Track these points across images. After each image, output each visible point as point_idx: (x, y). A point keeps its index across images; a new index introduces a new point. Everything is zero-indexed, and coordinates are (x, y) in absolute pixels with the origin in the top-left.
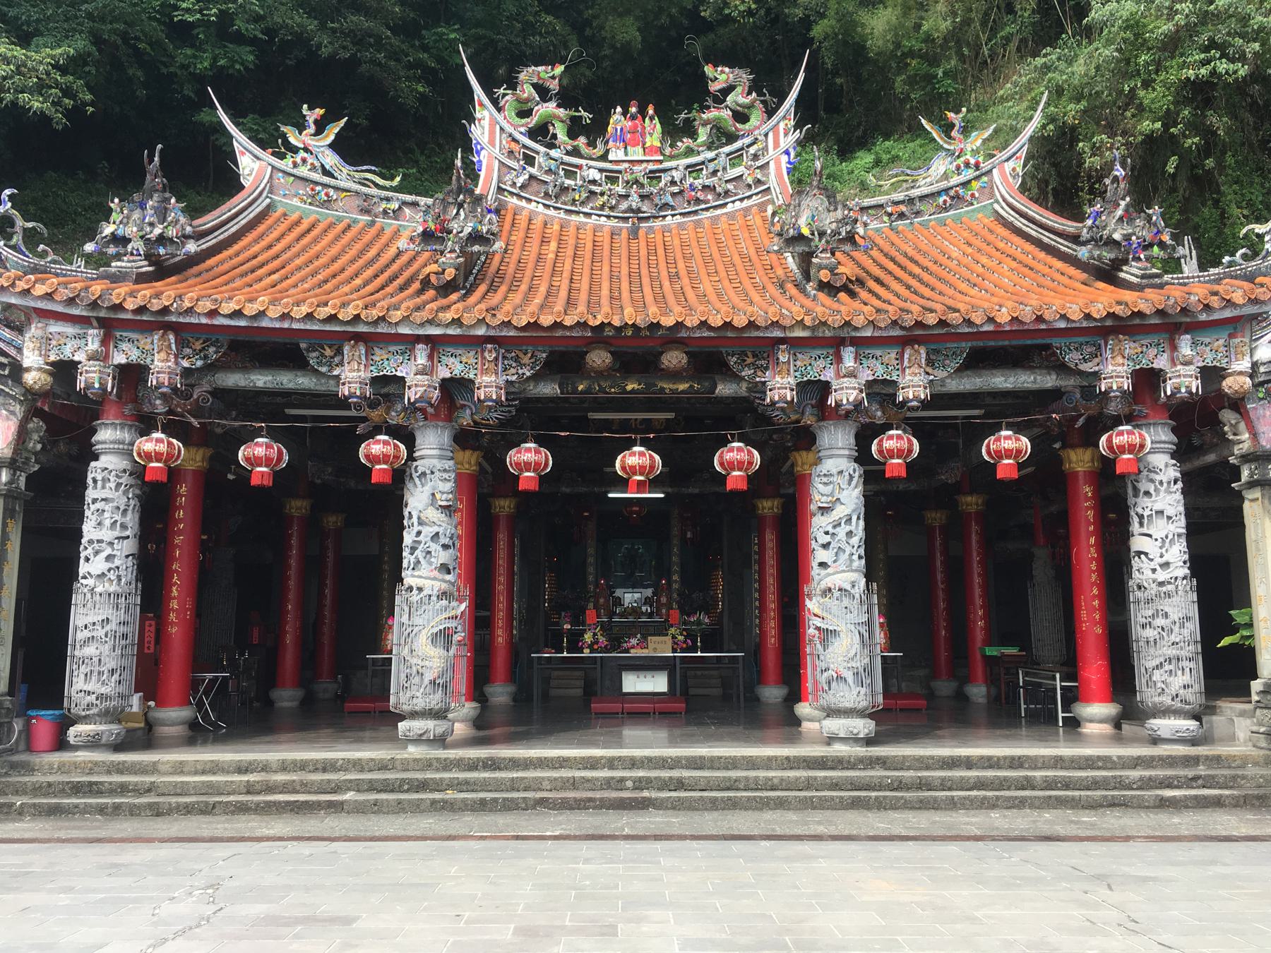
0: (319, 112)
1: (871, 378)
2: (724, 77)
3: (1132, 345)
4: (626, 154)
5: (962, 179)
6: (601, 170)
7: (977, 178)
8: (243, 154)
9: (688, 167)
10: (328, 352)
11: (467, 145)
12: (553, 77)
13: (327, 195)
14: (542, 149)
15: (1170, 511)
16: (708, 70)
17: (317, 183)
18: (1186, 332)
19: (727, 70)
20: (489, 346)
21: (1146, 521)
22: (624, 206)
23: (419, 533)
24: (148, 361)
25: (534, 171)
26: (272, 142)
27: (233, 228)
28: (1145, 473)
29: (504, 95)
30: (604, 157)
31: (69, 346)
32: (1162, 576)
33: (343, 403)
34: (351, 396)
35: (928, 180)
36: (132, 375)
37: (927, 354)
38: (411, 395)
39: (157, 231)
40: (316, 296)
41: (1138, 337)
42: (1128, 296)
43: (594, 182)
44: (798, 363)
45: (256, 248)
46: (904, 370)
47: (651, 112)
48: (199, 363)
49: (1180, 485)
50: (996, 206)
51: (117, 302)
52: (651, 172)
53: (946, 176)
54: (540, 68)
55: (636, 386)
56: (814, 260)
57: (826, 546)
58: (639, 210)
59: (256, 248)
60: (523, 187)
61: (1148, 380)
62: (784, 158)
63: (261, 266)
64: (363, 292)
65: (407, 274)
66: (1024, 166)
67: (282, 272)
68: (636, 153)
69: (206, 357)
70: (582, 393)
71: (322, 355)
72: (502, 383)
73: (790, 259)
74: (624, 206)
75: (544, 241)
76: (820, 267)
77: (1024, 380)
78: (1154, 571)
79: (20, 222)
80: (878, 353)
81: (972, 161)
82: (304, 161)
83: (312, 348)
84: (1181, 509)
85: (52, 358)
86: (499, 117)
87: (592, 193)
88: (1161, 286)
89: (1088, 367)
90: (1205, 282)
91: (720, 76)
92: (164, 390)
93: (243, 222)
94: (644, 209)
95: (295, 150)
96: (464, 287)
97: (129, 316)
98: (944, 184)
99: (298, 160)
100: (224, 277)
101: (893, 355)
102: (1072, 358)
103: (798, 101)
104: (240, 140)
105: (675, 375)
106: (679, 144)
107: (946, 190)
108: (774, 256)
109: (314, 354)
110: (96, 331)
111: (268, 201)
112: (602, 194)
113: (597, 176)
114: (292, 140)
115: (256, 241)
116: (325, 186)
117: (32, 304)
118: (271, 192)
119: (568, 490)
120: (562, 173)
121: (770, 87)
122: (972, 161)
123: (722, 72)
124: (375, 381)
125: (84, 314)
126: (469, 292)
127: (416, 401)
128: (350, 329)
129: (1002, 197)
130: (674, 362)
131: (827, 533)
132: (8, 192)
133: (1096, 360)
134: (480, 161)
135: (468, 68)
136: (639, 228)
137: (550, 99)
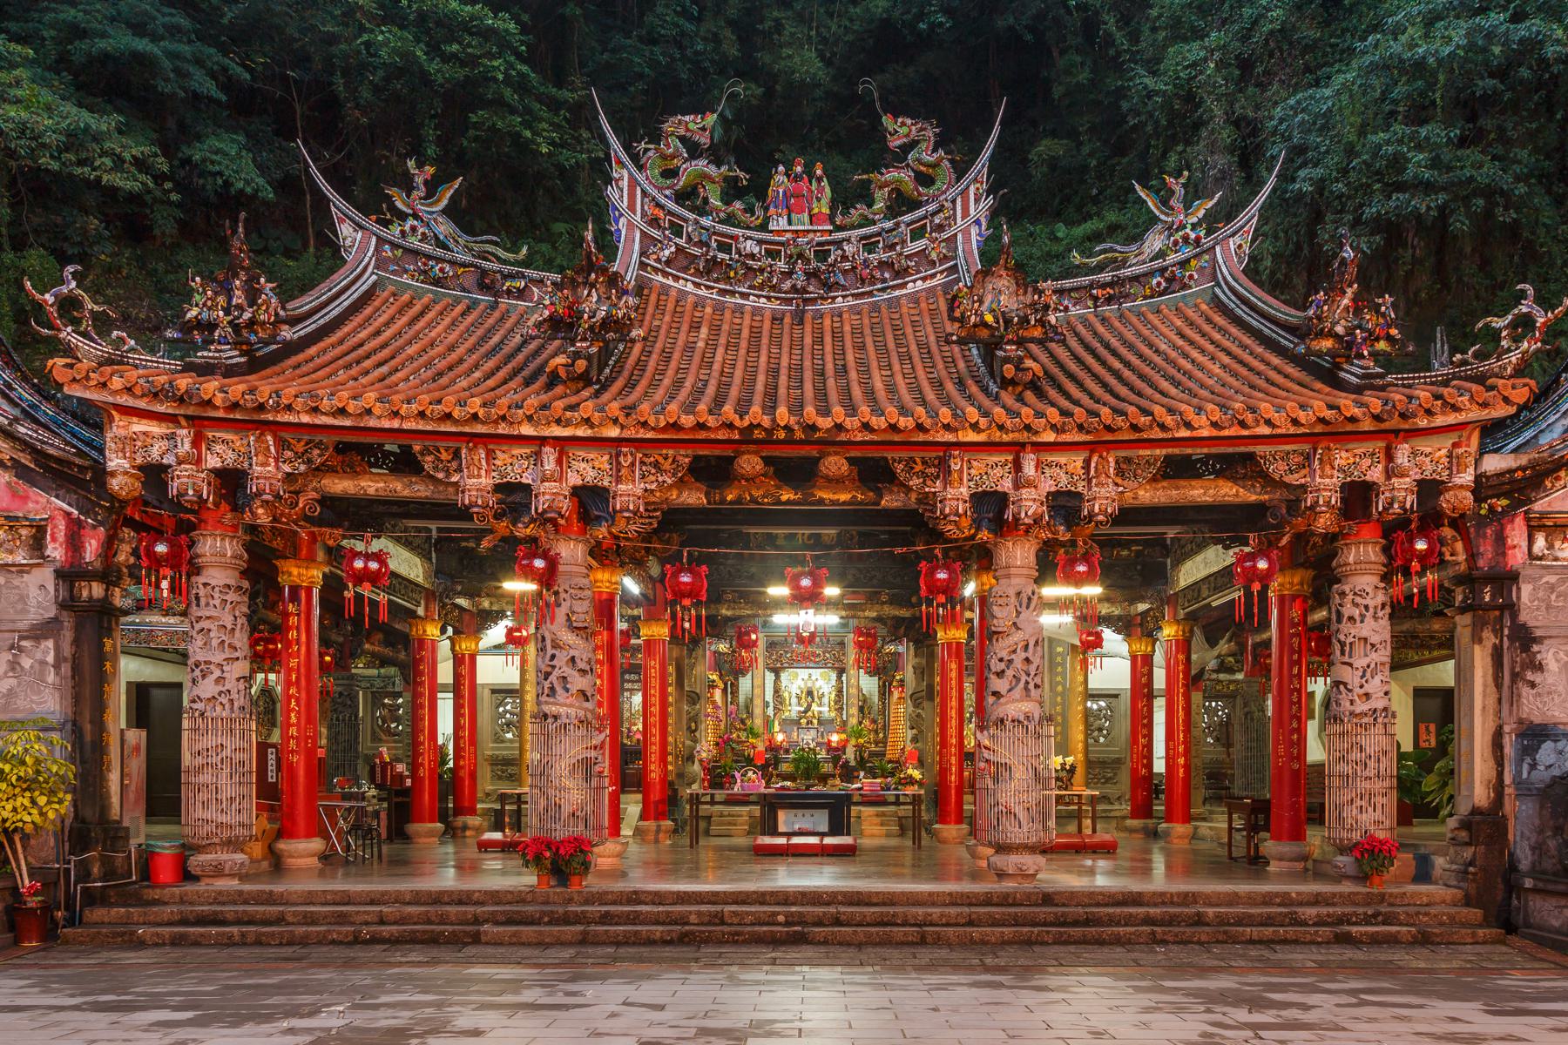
0: (430, 170)
1: (1053, 489)
2: (905, 130)
3: (1344, 454)
4: (790, 223)
5: (1179, 257)
6: (760, 242)
7: (1196, 256)
8: (341, 221)
9: (862, 238)
10: (444, 456)
11: (602, 213)
12: (703, 129)
13: (442, 270)
14: (691, 216)
15: (1375, 639)
16: (887, 121)
17: (429, 257)
18: (1405, 440)
19: (909, 121)
20: (625, 450)
21: (1347, 648)
22: (787, 285)
23: (553, 657)
24: (246, 465)
25: (682, 242)
26: (375, 207)
27: (335, 311)
28: (1351, 597)
29: (646, 150)
30: (763, 227)
31: (156, 447)
32: (1361, 707)
33: (464, 513)
34: (471, 505)
35: (1141, 258)
36: (231, 482)
37: (1117, 462)
38: (542, 503)
39: (247, 315)
40: (429, 391)
41: (1350, 446)
42: (1346, 401)
43: (752, 256)
44: (973, 472)
45: (363, 335)
46: (1090, 481)
47: (819, 172)
48: (303, 468)
49: (1388, 610)
50: (1217, 290)
51: (206, 398)
52: (819, 244)
53: (1161, 254)
54: (687, 118)
55: (792, 497)
56: (1000, 353)
57: (1000, 674)
58: (804, 290)
59: (363, 335)
60: (668, 262)
61: (1357, 496)
62: (974, 231)
63: (368, 356)
64: (483, 387)
65: (533, 366)
66: (1254, 240)
67: (393, 363)
68: (802, 222)
69: (309, 461)
70: (731, 503)
71: (439, 459)
72: (639, 492)
73: (975, 351)
74: (787, 285)
75: (695, 327)
76: (1007, 360)
77: (1227, 492)
78: (1352, 702)
79: (89, 305)
80: (1063, 460)
81: (1193, 236)
82: (414, 229)
83: (426, 451)
84: (1388, 636)
85: (139, 461)
86: (640, 177)
87: (749, 268)
88: (1383, 388)
89: (1295, 479)
90: (1432, 383)
91: (899, 129)
92: (265, 497)
93: (346, 304)
94: (811, 288)
95: (402, 217)
96: (598, 381)
97: (221, 414)
98: (1158, 263)
99: (407, 228)
100: (327, 369)
101: (1079, 464)
102: (1277, 469)
103: (992, 158)
104: (338, 204)
105: (835, 482)
106: (852, 211)
107: (1163, 270)
108: (956, 349)
109: (429, 458)
110: (184, 432)
111: (374, 277)
112: (762, 270)
113: (756, 250)
114: (399, 204)
115: (362, 326)
116: (439, 260)
117: (110, 399)
118: (377, 267)
119: (729, 613)
120: (714, 245)
121: (959, 141)
122: (1193, 236)
123: (903, 124)
124: (498, 488)
125: (170, 411)
126: (604, 387)
127: (545, 511)
128: (467, 429)
129: (1224, 279)
130: (834, 469)
131: (1001, 660)
132: (70, 269)
133: (1304, 472)
134: (619, 230)
135: (603, 118)
136: (804, 311)
137: (700, 156)
